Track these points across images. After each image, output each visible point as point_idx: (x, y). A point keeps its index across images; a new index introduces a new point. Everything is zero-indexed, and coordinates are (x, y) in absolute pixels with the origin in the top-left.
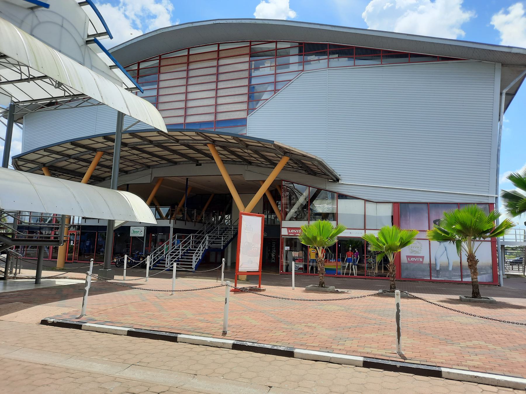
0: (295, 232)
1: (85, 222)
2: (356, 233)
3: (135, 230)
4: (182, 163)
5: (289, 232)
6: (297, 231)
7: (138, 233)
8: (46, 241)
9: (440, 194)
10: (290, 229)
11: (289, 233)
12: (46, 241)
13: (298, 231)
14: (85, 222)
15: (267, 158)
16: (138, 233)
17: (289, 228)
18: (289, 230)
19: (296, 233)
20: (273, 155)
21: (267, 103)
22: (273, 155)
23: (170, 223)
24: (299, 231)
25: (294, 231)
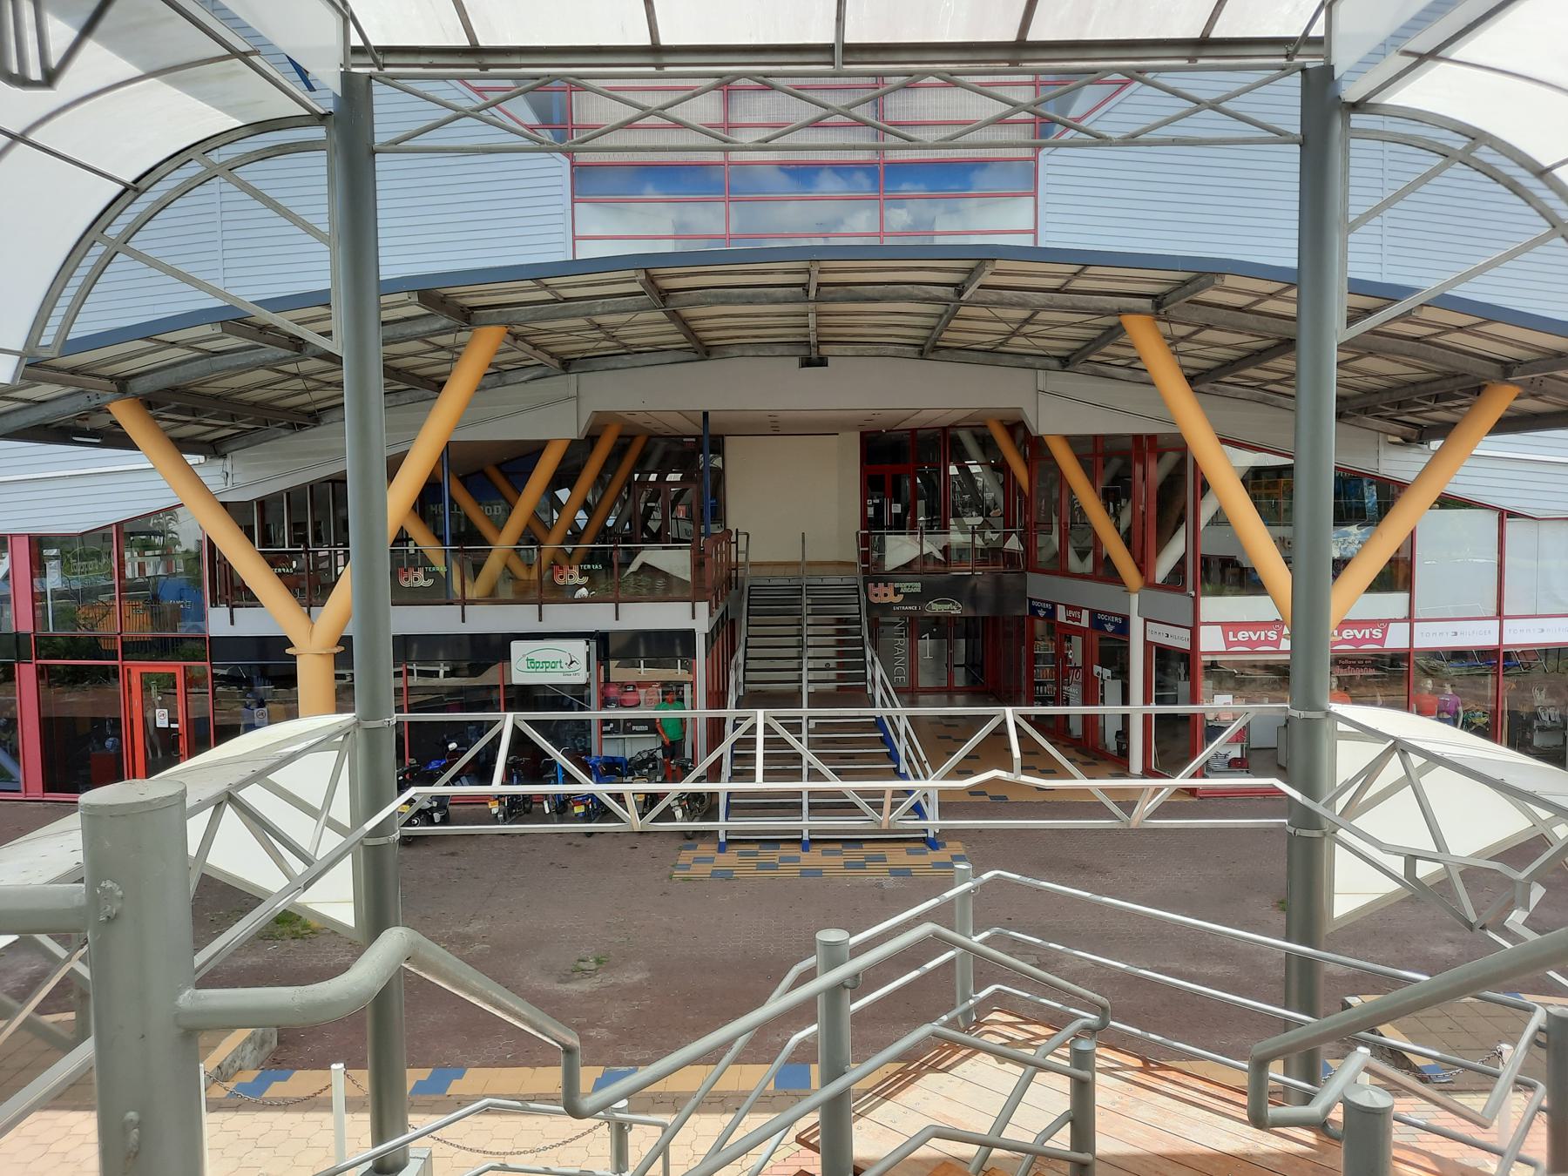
0: (1359, 636)
1: (232, 623)
2: (1473, 632)
3: (537, 657)
4: (736, 351)
5: (1231, 638)
6: (1263, 633)
7: (558, 669)
8: (848, 832)
9: (52, 484)
10: (1233, 628)
11: (1228, 643)
12: (848, 832)
13: (1371, 633)
14: (232, 623)
15: (413, 374)
16: (558, 669)
17: (1228, 626)
18: (1231, 633)
19: (1259, 642)
20: (263, 375)
21: (1105, 118)
22: (263, 375)
23: (694, 618)
24: (1269, 634)
25: (1356, 631)
